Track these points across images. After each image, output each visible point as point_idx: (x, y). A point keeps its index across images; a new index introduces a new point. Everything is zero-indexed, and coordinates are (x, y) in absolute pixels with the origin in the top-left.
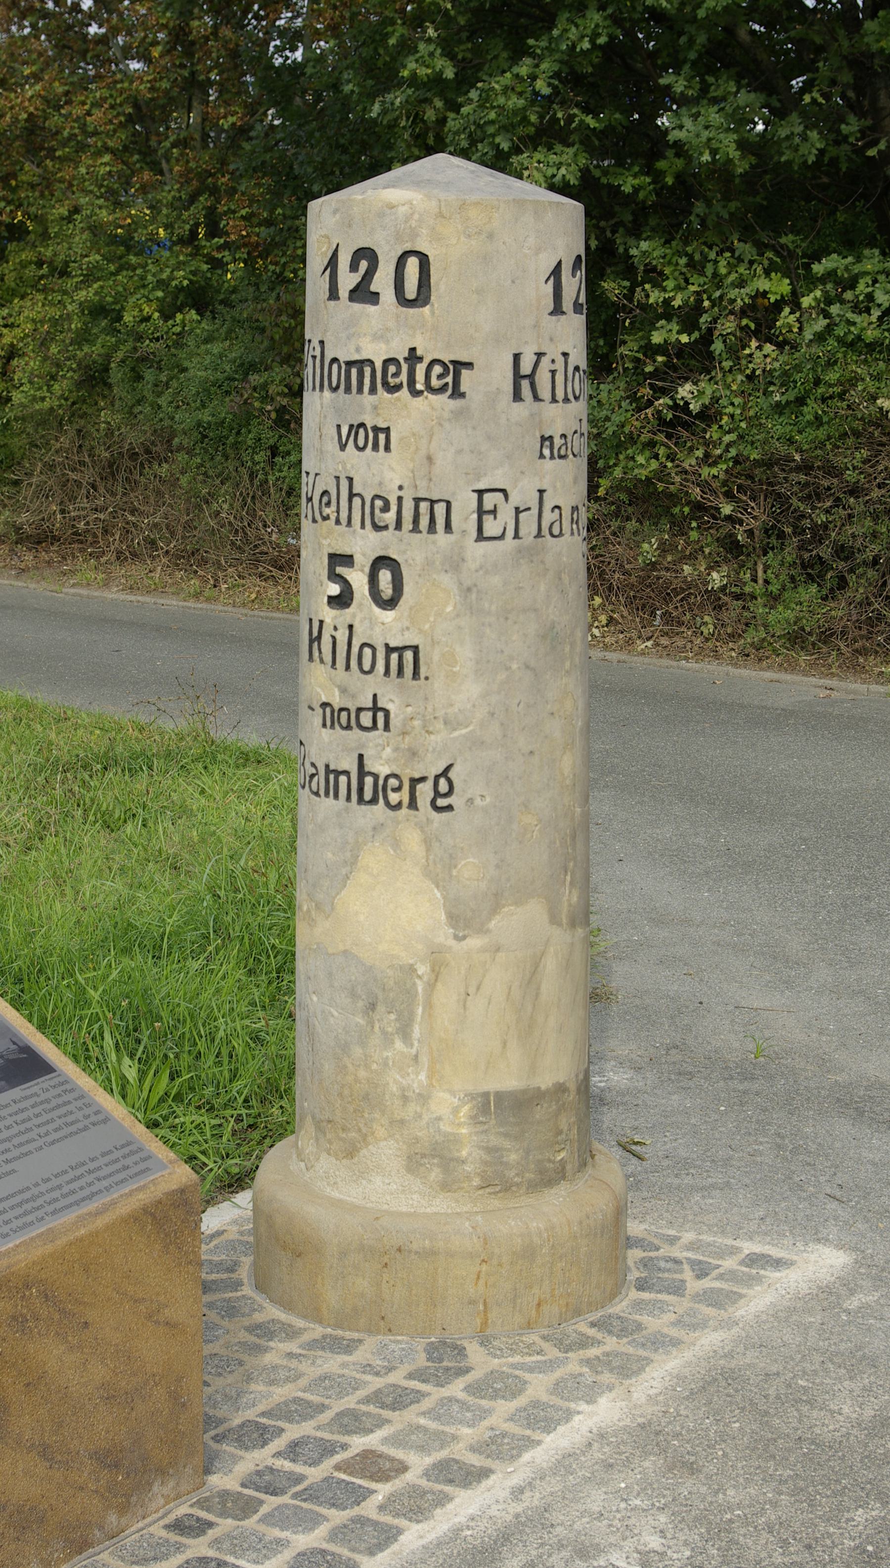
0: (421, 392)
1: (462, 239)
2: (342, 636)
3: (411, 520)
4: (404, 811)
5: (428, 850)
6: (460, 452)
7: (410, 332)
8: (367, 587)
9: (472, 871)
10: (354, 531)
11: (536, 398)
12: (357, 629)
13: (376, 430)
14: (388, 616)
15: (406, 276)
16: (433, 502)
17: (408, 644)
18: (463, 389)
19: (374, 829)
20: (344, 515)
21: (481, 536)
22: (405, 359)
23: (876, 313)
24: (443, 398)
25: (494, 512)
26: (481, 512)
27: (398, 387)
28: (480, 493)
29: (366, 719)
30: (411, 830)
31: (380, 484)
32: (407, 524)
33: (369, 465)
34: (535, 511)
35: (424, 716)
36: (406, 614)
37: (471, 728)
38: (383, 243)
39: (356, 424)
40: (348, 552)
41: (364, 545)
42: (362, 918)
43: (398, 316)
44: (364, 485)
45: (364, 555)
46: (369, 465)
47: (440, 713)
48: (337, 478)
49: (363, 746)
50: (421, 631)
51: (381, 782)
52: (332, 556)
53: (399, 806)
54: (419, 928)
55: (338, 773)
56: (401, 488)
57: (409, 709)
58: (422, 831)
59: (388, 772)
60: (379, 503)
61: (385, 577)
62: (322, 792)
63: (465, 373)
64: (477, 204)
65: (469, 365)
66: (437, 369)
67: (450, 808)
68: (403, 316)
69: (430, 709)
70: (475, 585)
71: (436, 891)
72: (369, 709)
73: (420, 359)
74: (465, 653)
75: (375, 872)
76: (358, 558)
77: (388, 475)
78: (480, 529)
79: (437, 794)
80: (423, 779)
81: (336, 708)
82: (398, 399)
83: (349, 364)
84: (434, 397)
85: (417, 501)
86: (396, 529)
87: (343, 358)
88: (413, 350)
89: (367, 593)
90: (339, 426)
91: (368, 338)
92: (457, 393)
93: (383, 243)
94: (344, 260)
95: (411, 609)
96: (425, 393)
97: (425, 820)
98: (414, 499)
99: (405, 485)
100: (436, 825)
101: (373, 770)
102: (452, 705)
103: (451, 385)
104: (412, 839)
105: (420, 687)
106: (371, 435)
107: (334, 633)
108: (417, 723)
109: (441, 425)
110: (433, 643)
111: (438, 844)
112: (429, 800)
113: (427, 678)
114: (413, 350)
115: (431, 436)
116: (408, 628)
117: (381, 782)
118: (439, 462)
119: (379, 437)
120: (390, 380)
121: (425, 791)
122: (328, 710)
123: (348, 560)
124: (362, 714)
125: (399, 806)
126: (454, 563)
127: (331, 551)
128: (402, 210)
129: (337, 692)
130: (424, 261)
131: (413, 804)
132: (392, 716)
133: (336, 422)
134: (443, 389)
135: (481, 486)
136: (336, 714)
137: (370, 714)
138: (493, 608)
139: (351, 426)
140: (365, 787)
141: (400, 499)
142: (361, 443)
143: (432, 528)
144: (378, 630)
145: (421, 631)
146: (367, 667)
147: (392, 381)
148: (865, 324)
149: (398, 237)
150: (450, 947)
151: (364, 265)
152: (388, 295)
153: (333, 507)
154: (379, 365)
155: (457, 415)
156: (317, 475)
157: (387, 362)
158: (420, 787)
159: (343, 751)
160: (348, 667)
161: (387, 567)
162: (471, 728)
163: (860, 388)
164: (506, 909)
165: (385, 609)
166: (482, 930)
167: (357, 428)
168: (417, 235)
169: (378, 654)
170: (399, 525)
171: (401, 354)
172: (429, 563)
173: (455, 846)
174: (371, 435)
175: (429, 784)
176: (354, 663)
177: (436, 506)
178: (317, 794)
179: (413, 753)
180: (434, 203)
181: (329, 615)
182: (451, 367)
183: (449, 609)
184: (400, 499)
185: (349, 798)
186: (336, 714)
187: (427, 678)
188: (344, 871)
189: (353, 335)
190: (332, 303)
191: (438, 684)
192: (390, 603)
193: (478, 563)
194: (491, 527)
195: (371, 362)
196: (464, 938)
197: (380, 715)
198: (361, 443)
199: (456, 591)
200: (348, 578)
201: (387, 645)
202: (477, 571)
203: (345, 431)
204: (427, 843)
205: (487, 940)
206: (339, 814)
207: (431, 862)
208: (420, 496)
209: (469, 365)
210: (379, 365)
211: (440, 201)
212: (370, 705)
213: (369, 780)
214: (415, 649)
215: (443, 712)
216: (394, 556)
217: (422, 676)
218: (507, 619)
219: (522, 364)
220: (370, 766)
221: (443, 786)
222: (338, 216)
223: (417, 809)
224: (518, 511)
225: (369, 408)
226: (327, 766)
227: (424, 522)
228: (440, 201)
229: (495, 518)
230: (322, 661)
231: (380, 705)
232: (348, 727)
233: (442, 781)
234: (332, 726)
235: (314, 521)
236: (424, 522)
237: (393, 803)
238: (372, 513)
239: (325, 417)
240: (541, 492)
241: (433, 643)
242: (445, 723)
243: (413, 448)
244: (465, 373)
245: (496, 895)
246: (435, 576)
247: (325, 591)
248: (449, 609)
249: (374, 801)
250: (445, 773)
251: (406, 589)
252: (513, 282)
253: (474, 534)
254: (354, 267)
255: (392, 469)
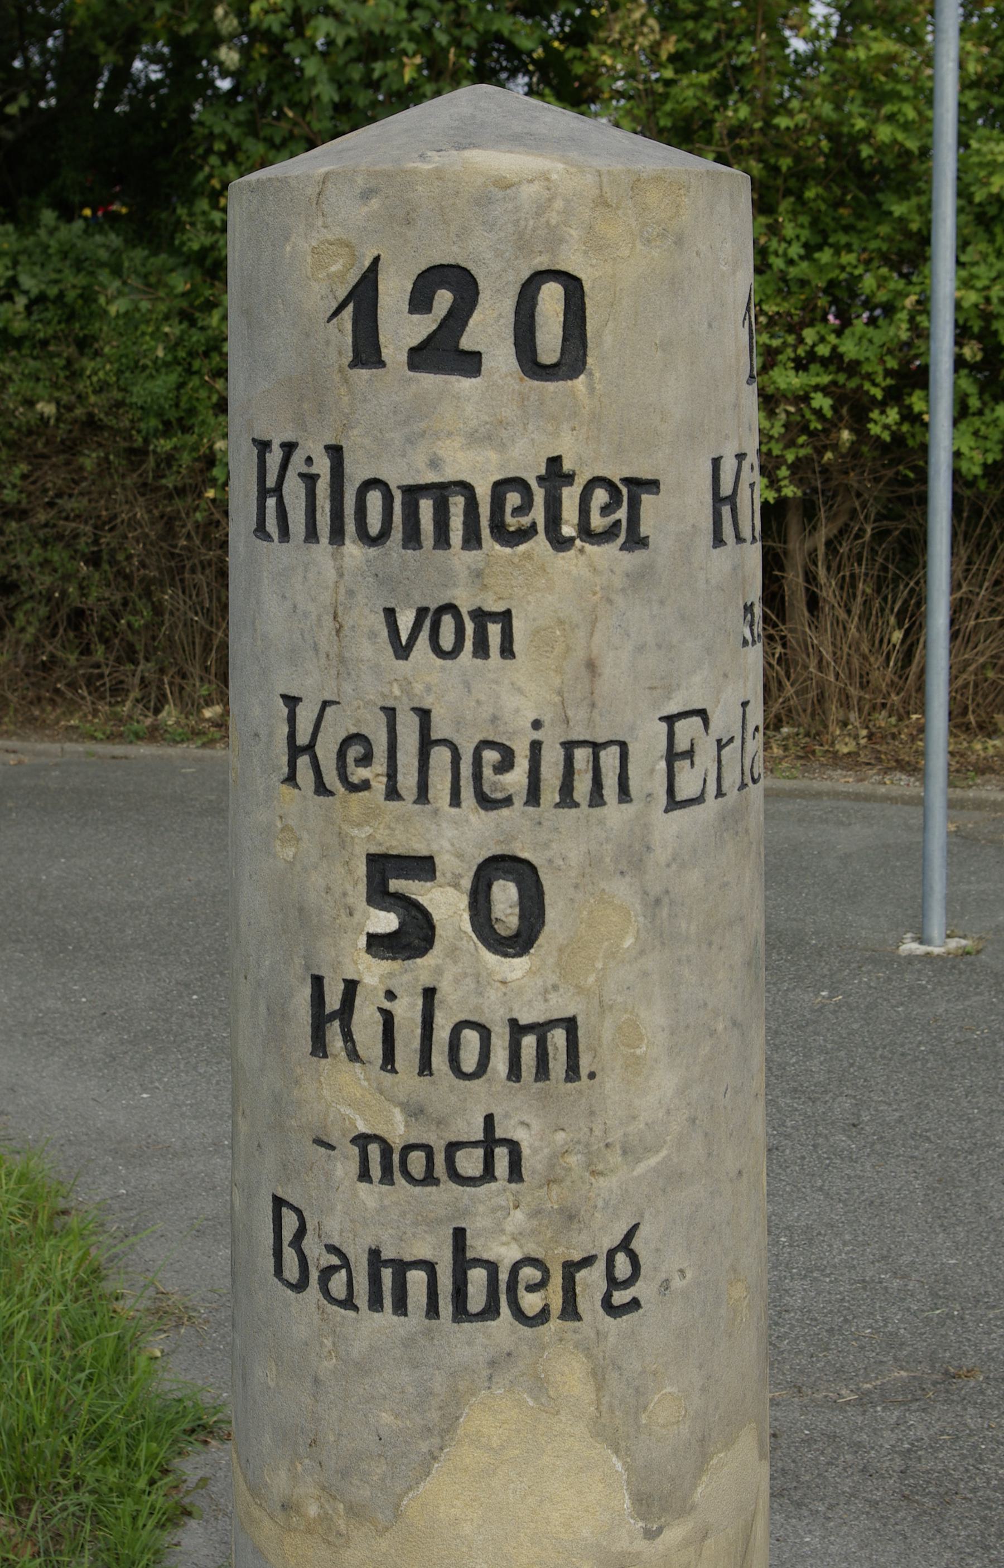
0: (571, 540)
1: (639, 246)
2: (407, 1012)
3: (557, 783)
4: (555, 1324)
5: (599, 1388)
6: (641, 648)
7: (550, 428)
8: (466, 916)
9: (668, 1412)
10: (436, 812)
11: (739, 539)
12: (446, 991)
13: (481, 616)
14: (516, 968)
15: (539, 319)
16: (596, 747)
17: (556, 1016)
18: (644, 530)
19: (492, 1363)
20: (408, 780)
21: (673, 803)
22: (540, 479)
23: (21, 301)
24: (611, 550)
25: (689, 754)
26: (672, 756)
27: (526, 534)
28: (670, 720)
29: (470, 1163)
30: (565, 1360)
31: (494, 719)
32: (550, 793)
33: (468, 686)
34: (738, 742)
35: (587, 1145)
36: (551, 961)
37: (664, 1153)
38: (489, 255)
39: (433, 606)
40: (421, 849)
41: (457, 836)
42: (467, 1529)
43: (523, 398)
44: (459, 723)
45: (460, 856)
46: (468, 686)
47: (616, 1136)
48: (390, 713)
49: (465, 1213)
50: (580, 990)
51: (503, 1276)
52: (373, 859)
53: (543, 1315)
54: (585, 1532)
55: (401, 1267)
56: (537, 725)
57: (560, 1136)
58: (589, 1356)
59: (518, 1256)
60: (491, 756)
61: (505, 895)
62: (362, 1299)
63: (647, 499)
64: (658, 179)
65: (652, 485)
66: (601, 496)
67: (635, 1304)
68: (533, 397)
69: (598, 1132)
70: (667, 892)
71: (614, 1459)
72: (475, 1144)
73: (569, 478)
74: (654, 1018)
75: (495, 1442)
76: (444, 862)
77: (510, 701)
78: (671, 791)
79: (613, 1283)
80: (588, 1261)
81: (397, 1143)
82: (528, 556)
83: (413, 492)
84: (595, 548)
85: (569, 746)
86: (527, 803)
87: (396, 477)
88: (555, 462)
89: (467, 927)
90: (390, 614)
91: (458, 442)
92: (636, 541)
93: (489, 255)
94: (394, 291)
95: (561, 950)
96: (578, 542)
97: (593, 1335)
98: (564, 744)
99: (546, 719)
100: (612, 1339)
101: (485, 1256)
102: (634, 1118)
103: (624, 523)
104: (571, 1375)
105: (580, 1092)
106: (469, 627)
107: (387, 1005)
108: (573, 1160)
109: (610, 601)
110: (603, 1009)
111: (615, 1375)
112: (599, 1297)
113: (592, 1076)
114: (555, 462)
115: (594, 622)
116: (555, 988)
117: (503, 1276)
118: (607, 671)
119: (489, 631)
120: (509, 519)
121: (592, 1282)
122: (374, 1151)
123: (423, 867)
124: (460, 1155)
125: (543, 1315)
126: (634, 857)
127: (373, 850)
128: (529, 192)
129: (398, 1116)
130: (573, 287)
131: (570, 1311)
132: (526, 1151)
133: (381, 604)
134: (609, 534)
135: (673, 709)
136: (396, 1158)
137: (480, 1152)
138: (693, 928)
139: (422, 612)
140: (468, 1288)
141: (536, 746)
142: (447, 641)
143: (597, 798)
144: (493, 995)
145: (580, 990)
146: (469, 1065)
147: (512, 522)
148: (10, 315)
149: (523, 245)
150: (639, 1554)
151: (444, 299)
152: (500, 356)
153: (380, 765)
154: (483, 493)
155: (638, 580)
156: (325, 704)
157: (501, 488)
158: (581, 1276)
159: (416, 1224)
160: (425, 1067)
161: (507, 875)
162: (664, 1153)
163: (11, 390)
164: (714, 1461)
165: (506, 955)
166: (685, 1510)
167: (431, 617)
168: (561, 240)
169: (494, 1039)
170: (533, 796)
171: (532, 471)
172: (593, 861)
173: (643, 1372)
174: (469, 627)
175: (601, 1265)
176: (439, 1060)
177: (603, 754)
178: (348, 1303)
179: (570, 1216)
180: (590, 179)
181: (373, 973)
182: (625, 491)
183: (628, 942)
184: (536, 746)
185: (433, 1310)
186: (396, 1158)
187: (592, 1076)
188: (424, 1447)
189: (423, 434)
190: (364, 373)
191: (610, 1083)
192: (520, 942)
193: (670, 850)
194: (687, 785)
195: (466, 488)
196: (660, 1530)
197: (501, 1154)
198: (447, 641)
199: (638, 907)
200: (422, 900)
201: (513, 1022)
202: (668, 865)
203: (406, 621)
204: (598, 1376)
205: (691, 1525)
206: (408, 1342)
207: (604, 1409)
208: (575, 737)
209: (652, 485)
210: (483, 493)
211: (600, 175)
212: (480, 1136)
213: (477, 1276)
214: (570, 1025)
215: (620, 1133)
216: (524, 855)
217: (584, 1072)
218: (710, 944)
219: (722, 476)
220: (477, 1247)
221: (622, 1266)
222: (375, 203)
223: (579, 1318)
224: (720, 745)
225: (463, 574)
226: (374, 1254)
227: (582, 786)
228: (600, 175)
229: (692, 764)
230: (354, 1055)
231: (499, 1134)
232: (429, 1179)
233: (621, 1258)
234: (387, 1177)
235: (321, 789)
236: (582, 786)
237: (530, 1313)
238: (477, 776)
239: (351, 593)
240: (745, 704)
241: (603, 1009)
242: (625, 1153)
243: (559, 649)
244: (647, 499)
245: (702, 1440)
246: (603, 885)
247: (361, 926)
248: (628, 942)
249: (490, 1311)
250: (625, 1245)
251: (551, 914)
252: (710, 326)
253: (663, 799)
254: (420, 300)
255: (520, 691)
